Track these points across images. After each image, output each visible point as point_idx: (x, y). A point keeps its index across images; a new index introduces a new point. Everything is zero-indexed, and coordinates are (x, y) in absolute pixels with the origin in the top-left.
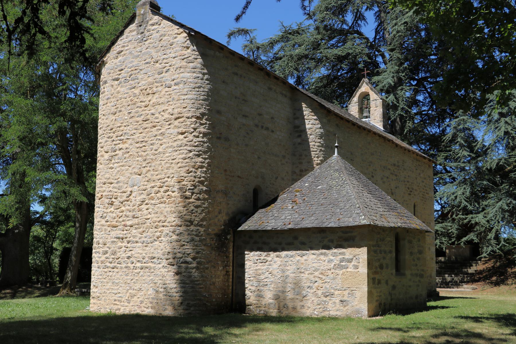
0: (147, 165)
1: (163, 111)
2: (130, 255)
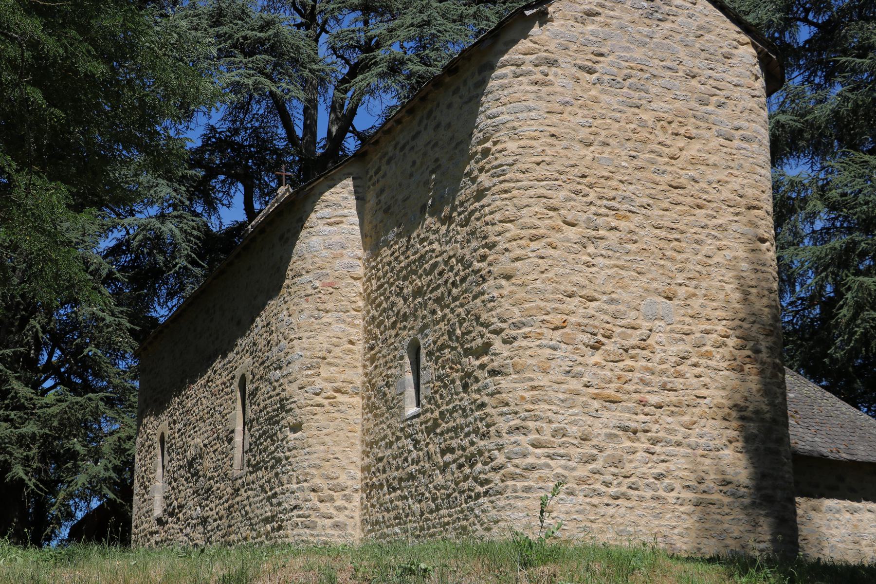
0: (687, 282)
2: (664, 472)
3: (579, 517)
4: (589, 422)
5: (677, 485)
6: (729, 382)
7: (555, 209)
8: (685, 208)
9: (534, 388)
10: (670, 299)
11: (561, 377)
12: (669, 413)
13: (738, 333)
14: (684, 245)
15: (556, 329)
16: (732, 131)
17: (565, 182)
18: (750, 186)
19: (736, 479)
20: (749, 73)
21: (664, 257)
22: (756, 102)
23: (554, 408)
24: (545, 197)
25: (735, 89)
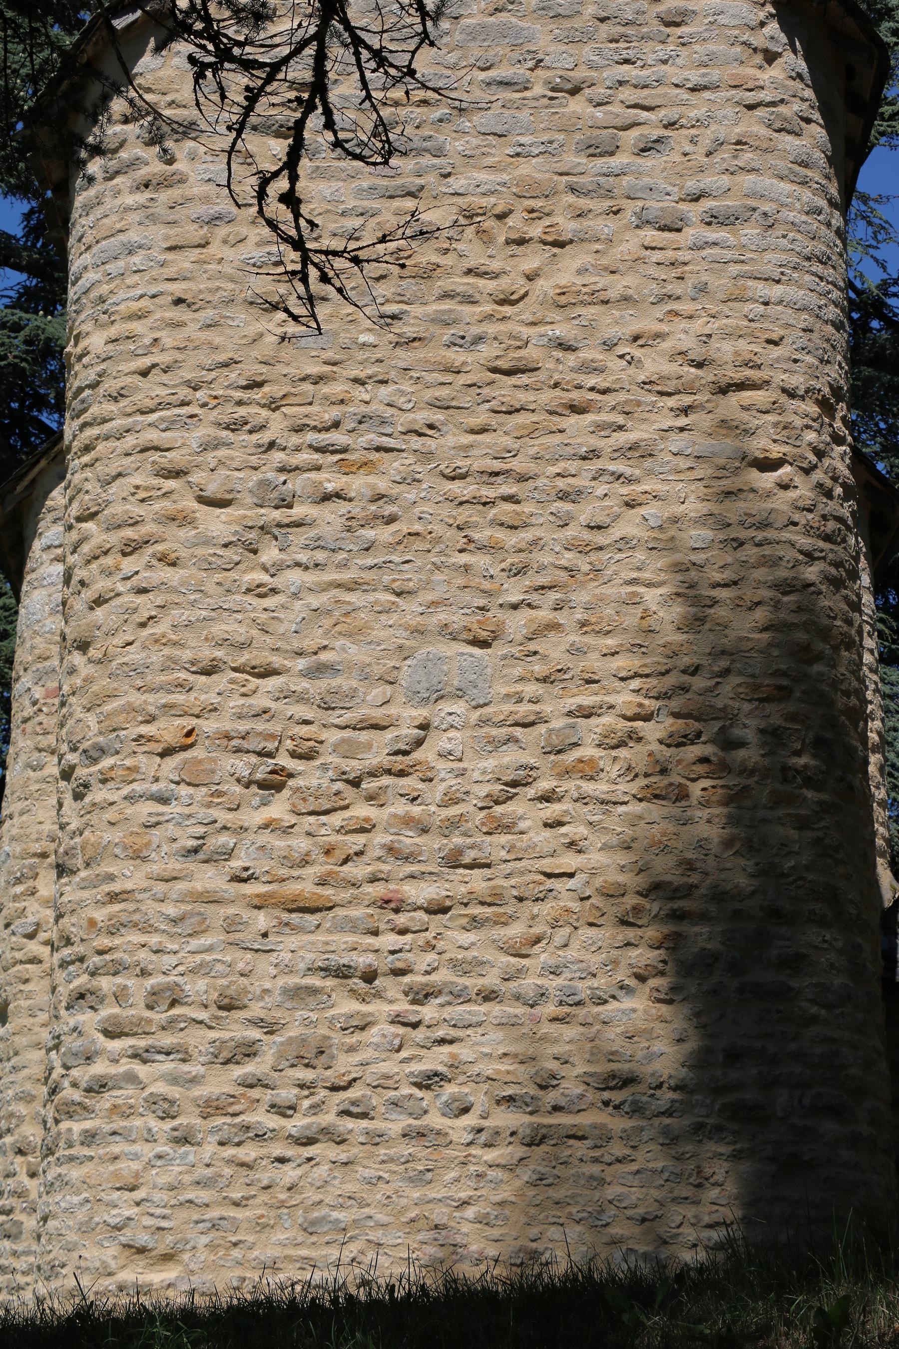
0: (534, 598)
1: (636, 338)
2: (441, 1069)
3: (203, 1196)
4: (241, 966)
5: (479, 1099)
6: (641, 830)
7: (177, 474)
8: (534, 418)
9: (113, 897)
10: (484, 644)
11: (175, 865)
12: (464, 921)
13: (675, 704)
14: (527, 508)
15: (165, 753)
16: (683, 206)
17: (204, 405)
18: (730, 335)
19: (649, 1069)
20: (738, 49)
21: (469, 545)
22: (761, 121)
23: (154, 940)
24: (157, 449)
25: (694, 98)
